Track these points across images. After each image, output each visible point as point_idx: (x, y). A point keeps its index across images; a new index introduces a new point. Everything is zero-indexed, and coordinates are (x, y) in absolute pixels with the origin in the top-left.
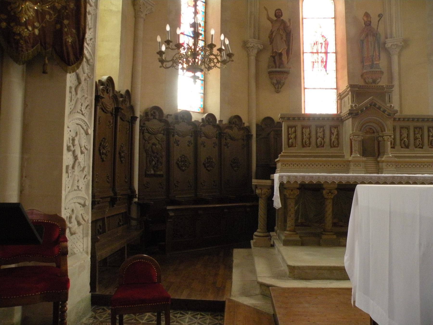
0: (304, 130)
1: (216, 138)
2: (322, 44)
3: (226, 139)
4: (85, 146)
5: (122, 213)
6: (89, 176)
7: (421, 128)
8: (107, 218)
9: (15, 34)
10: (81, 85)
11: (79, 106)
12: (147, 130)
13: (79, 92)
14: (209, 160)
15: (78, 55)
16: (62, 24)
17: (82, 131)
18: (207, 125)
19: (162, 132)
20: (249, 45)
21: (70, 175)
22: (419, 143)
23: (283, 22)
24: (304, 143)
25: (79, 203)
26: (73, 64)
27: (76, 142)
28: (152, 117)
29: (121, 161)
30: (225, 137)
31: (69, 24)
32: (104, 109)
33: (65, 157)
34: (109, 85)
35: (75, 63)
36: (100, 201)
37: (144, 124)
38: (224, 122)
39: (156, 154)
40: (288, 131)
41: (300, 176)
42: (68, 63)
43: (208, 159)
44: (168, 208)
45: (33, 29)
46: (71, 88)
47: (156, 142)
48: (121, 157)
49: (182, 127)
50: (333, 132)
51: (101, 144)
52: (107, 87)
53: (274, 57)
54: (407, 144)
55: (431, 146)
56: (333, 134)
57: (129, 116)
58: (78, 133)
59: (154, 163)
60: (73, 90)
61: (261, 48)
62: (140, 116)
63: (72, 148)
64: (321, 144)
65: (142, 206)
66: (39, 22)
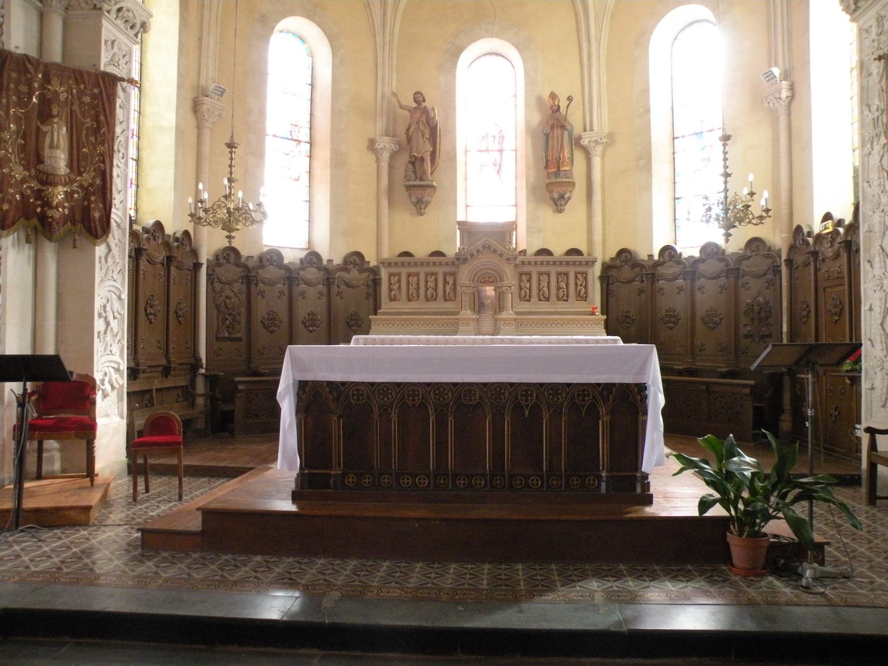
0: (410, 278)
1: (323, 285)
2: (494, 137)
3: (338, 286)
4: (118, 311)
5: (182, 387)
6: (124, 340)
7: (566, 274)
8: (156, 390)
9: (48, 217)
10: (112, 252)
11: (110, 273)
12: (218, 278)
13: (109, 260)
14: (311, 317)
15: (106, 228)
16: (89, 200)
17: (114, 297)
18: (307, 267)
19: (240, 281)
20: (377, 146)
21: (102, 340)
22: (564, 294)
23: (425, 111)
24: (411, 297)
25: (113, 368)
26: (101, 237)
27: (108, 308)
28: (225, 262)
29: (179, 322)
30: (336, 283)
31: (96, 200)
32: (150, 260)
33: (96, 324)
34: (156, 230)
35: (103, 236)
36: (146, 369)
37: (214, 271)
38: (336, 262)
39: (231, 310)
40: (390, 280)
41: (379, 339)
42: (97, 237)
43: (309, 315)
44: (237, 379)
45: (63, 210)
46: (100, 258)
47: (231, 295)
48: (178, 317)
49: (271, 273)
50: (448, 280)
51: (147, 303)
52: (155, 234)
53: (413, 163)
54: (547, 297)
55: (578, 297)
56: (448, 283)
57: (189, 263)
58: (110, 299)
59: (228, 322)
60: (103, 259)
61: (395, 149)
62: (208, 260)
63: (104, 314)
64: (433, 297)
65: (212, 380)
66: (68, 202)
